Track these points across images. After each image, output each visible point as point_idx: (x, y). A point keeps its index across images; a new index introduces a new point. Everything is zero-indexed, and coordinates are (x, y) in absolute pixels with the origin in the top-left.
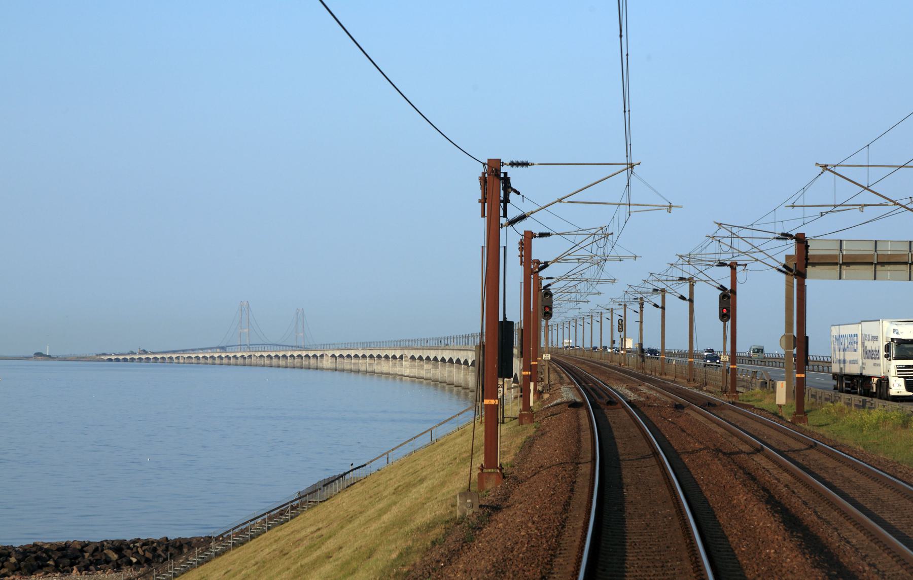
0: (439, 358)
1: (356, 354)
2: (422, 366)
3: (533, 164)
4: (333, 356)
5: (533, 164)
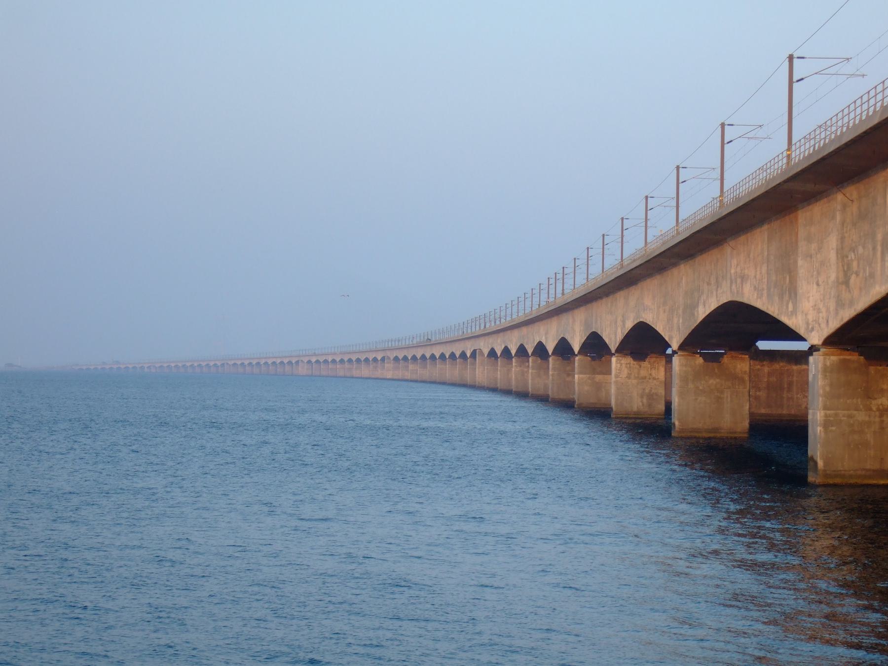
0: (428, 356)
1: (318, 360)
2: (408, 367)
3: (806, 58)
4: (309, 362)
5: (806, 58)
